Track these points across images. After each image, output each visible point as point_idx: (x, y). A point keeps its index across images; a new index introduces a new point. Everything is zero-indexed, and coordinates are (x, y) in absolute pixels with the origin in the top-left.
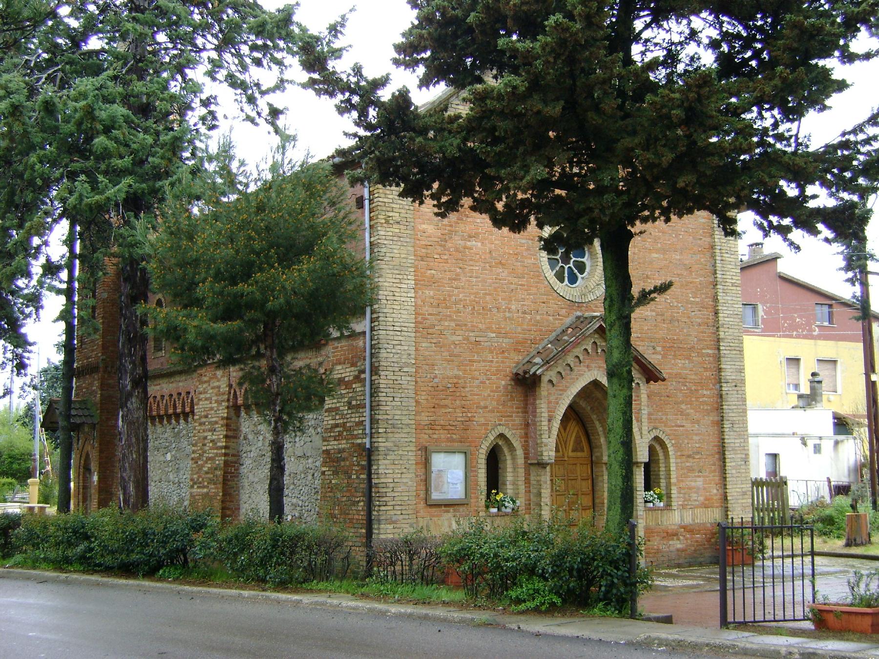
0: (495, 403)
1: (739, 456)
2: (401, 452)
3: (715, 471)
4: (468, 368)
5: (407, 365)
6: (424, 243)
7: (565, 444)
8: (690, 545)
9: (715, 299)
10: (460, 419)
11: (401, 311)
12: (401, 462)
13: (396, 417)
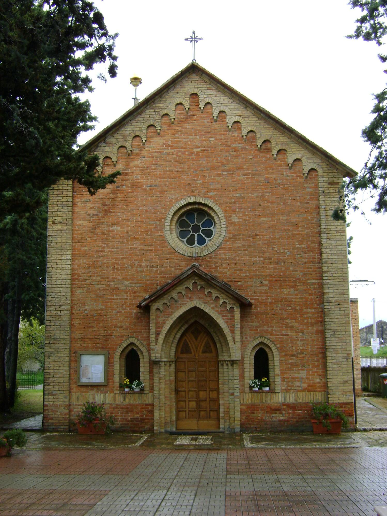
0: (128, 324)
1: (340, 355)
2: (59, 355)
3: (318, 366)
4: (109, 304)
5: (65, 304)
6: (80, 232)
7: (197, 348)
8: (292, 418)
9: (320, 244)
10: (102, 335)
11: (62, 273)
12: (59, 360)
13: (57, 335)
